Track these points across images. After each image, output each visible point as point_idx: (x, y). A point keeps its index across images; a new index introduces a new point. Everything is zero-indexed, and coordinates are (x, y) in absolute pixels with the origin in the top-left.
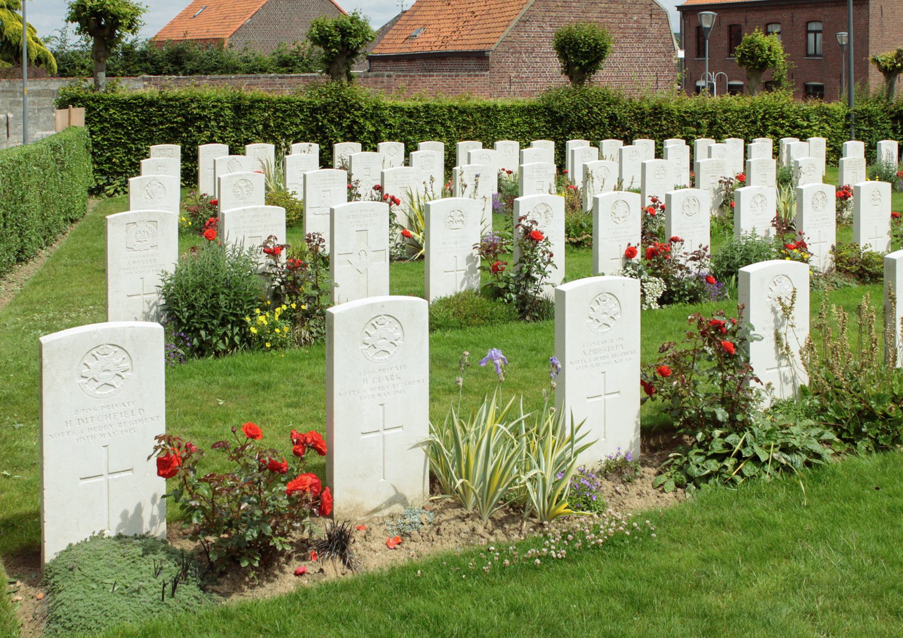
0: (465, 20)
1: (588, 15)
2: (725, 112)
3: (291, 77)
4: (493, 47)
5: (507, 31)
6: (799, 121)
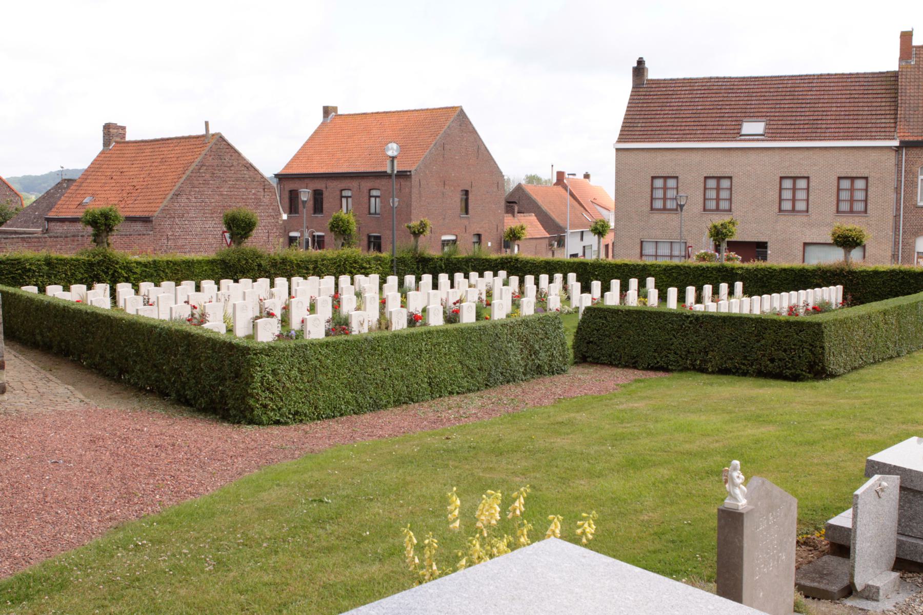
2: (323, 260)
3: (13, 238)
4: (156, 214)
6: (365, 265)
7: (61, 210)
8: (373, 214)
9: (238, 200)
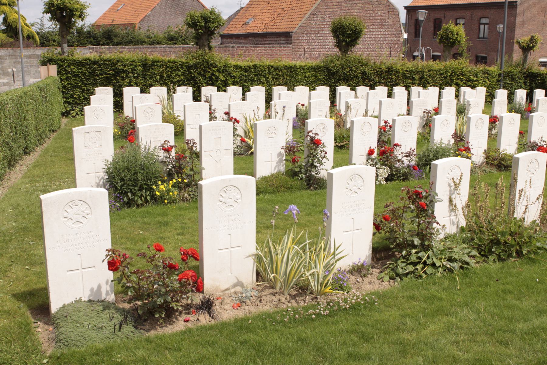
0: (278, 13)
2: (429, 71)
3: (176, 47)
4: (295, 30)
5: (303, 20)
6: (472, 77)
7: (231, 29)
8: (481, 38)
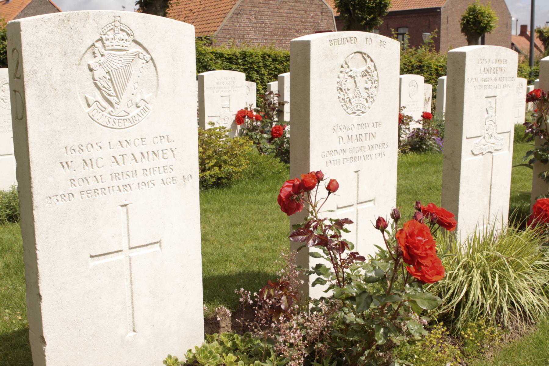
0: (185, 16)
1: (282, 11)
5: (225, 21)
9: (297, 23)
